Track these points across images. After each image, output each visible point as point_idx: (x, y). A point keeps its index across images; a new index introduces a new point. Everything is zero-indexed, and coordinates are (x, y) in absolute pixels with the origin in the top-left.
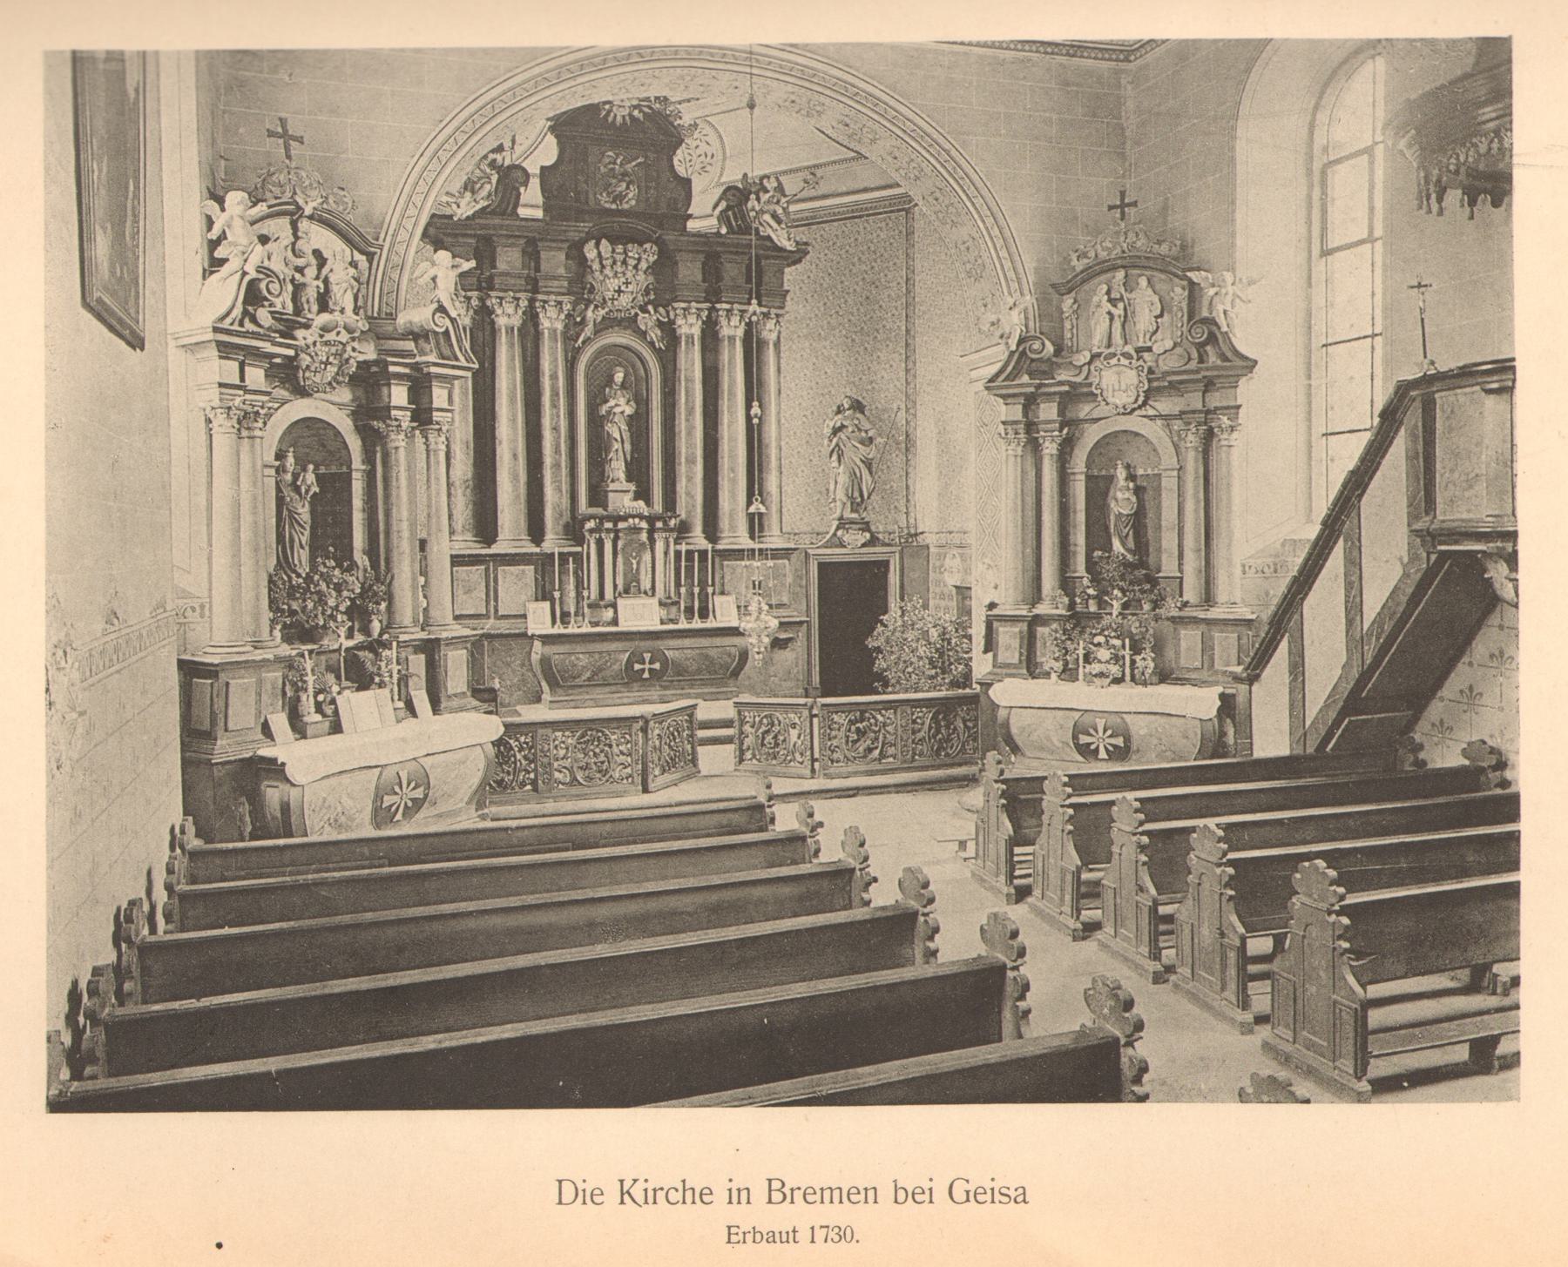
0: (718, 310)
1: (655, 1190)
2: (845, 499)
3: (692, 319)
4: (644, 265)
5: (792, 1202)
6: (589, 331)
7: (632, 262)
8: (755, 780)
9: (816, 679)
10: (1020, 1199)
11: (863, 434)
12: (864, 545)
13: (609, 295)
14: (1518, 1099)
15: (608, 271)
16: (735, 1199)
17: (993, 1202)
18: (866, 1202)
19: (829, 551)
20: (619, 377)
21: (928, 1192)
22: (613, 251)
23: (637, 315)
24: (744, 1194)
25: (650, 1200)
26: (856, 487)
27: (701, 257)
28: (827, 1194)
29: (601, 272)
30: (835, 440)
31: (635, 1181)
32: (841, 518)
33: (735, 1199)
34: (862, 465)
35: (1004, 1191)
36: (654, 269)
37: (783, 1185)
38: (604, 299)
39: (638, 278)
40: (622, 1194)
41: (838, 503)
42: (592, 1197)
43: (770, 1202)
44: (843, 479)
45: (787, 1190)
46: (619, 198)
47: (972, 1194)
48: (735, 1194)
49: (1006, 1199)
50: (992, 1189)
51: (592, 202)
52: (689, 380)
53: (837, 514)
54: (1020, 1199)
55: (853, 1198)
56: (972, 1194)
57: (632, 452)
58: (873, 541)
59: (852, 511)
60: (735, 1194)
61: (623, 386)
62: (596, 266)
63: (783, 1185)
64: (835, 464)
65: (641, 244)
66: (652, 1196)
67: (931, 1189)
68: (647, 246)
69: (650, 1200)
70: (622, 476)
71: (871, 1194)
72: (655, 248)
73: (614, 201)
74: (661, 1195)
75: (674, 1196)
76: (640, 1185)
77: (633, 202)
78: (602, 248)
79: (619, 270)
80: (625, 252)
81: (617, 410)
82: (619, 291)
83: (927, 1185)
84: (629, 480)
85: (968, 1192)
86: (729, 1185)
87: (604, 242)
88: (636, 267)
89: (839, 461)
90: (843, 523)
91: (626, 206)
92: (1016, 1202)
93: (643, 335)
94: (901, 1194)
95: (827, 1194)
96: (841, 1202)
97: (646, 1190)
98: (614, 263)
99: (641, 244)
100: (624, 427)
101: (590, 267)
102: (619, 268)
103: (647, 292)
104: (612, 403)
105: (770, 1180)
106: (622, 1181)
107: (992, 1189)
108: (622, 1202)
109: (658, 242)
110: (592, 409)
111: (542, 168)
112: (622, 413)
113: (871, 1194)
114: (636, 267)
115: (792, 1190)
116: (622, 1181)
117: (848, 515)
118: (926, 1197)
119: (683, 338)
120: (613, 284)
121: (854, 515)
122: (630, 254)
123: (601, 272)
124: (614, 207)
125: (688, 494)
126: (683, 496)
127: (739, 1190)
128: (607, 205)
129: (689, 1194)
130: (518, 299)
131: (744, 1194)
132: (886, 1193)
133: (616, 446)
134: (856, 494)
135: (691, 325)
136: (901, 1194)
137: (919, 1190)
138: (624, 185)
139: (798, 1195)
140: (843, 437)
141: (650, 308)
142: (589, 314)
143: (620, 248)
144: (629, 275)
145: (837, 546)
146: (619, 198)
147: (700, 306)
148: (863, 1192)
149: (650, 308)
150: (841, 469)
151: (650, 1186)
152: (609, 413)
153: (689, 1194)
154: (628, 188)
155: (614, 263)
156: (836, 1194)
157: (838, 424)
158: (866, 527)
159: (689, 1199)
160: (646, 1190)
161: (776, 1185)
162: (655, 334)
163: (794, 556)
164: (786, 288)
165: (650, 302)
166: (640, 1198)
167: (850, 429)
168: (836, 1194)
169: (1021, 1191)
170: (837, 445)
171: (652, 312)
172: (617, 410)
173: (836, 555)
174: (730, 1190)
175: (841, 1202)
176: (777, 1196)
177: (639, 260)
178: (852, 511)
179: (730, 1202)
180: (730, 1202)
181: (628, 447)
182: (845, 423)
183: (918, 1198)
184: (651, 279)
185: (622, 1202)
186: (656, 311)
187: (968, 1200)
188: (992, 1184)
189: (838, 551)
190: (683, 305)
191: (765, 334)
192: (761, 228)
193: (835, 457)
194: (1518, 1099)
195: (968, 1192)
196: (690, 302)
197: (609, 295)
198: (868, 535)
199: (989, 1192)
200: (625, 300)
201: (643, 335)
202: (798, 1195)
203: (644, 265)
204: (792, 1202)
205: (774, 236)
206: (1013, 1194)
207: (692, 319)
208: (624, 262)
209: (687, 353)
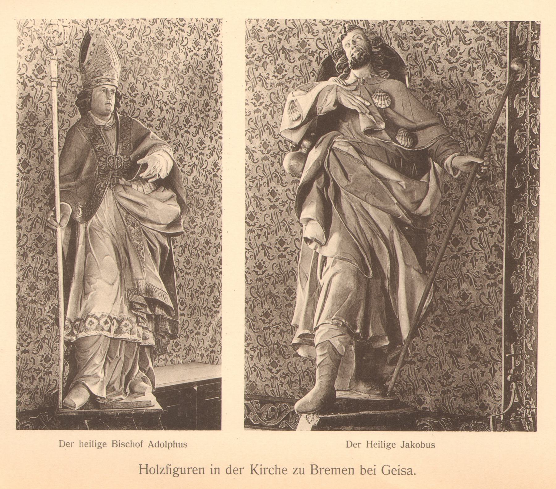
1: (265, 469)
8: (63, 164)
10: (409, 473)
11: (403, 141)
14: (534, 428)
16: (213, 472)
18: (200, 473)
24: (217, 470)
25: (263, 472)
28: (334, 470)
30: (314, 155)
31: (257, 465)
33: (213, 472)
35: (403, 470)
37: (317, 467)
40: (252, 470)
41: (319, 355)
42: (302, 472)
43: (312, 474)
45: (318, 469)
47: (391, 471)
49: (404, 473)
54: (409, 473)
56: (391, 471)
66: (265, 471)
69: (263, 472)
71: (202, 470)
74: (267, 471)
75: (272, 471)
76: (259, 467)
83: (373, 468)
85: (389, 470)
89: (326, 223)
94: (363, 471)
95: (334, 470)
97: (261, 469)
105: (312, 465)
106: (252, 465)
108: (252, 473)
113: (202, 470)
115: (321, 469)
116: (252, 465)
118: (373, 472)
127: (215, 469)
131: (217, 470)
132: (357, 470)
136: (363, 471)
137: (394, 470)
139: (323, 471)
151: (263, 467)
156: (338, 470)
159: (278, 472)
160: (261, 469)
161: (314, 467)
166: (259, 472)
168: (338, 470)
169: (410, 470)
176: (315, 471)
179: (212, 473)
180: (212, 473)
183: (345, 472)
185: (252, 473)
187: (389, 473)
188: (399, 467)
194: (534, 428)
202: (323, 471)
206: (407, 471)
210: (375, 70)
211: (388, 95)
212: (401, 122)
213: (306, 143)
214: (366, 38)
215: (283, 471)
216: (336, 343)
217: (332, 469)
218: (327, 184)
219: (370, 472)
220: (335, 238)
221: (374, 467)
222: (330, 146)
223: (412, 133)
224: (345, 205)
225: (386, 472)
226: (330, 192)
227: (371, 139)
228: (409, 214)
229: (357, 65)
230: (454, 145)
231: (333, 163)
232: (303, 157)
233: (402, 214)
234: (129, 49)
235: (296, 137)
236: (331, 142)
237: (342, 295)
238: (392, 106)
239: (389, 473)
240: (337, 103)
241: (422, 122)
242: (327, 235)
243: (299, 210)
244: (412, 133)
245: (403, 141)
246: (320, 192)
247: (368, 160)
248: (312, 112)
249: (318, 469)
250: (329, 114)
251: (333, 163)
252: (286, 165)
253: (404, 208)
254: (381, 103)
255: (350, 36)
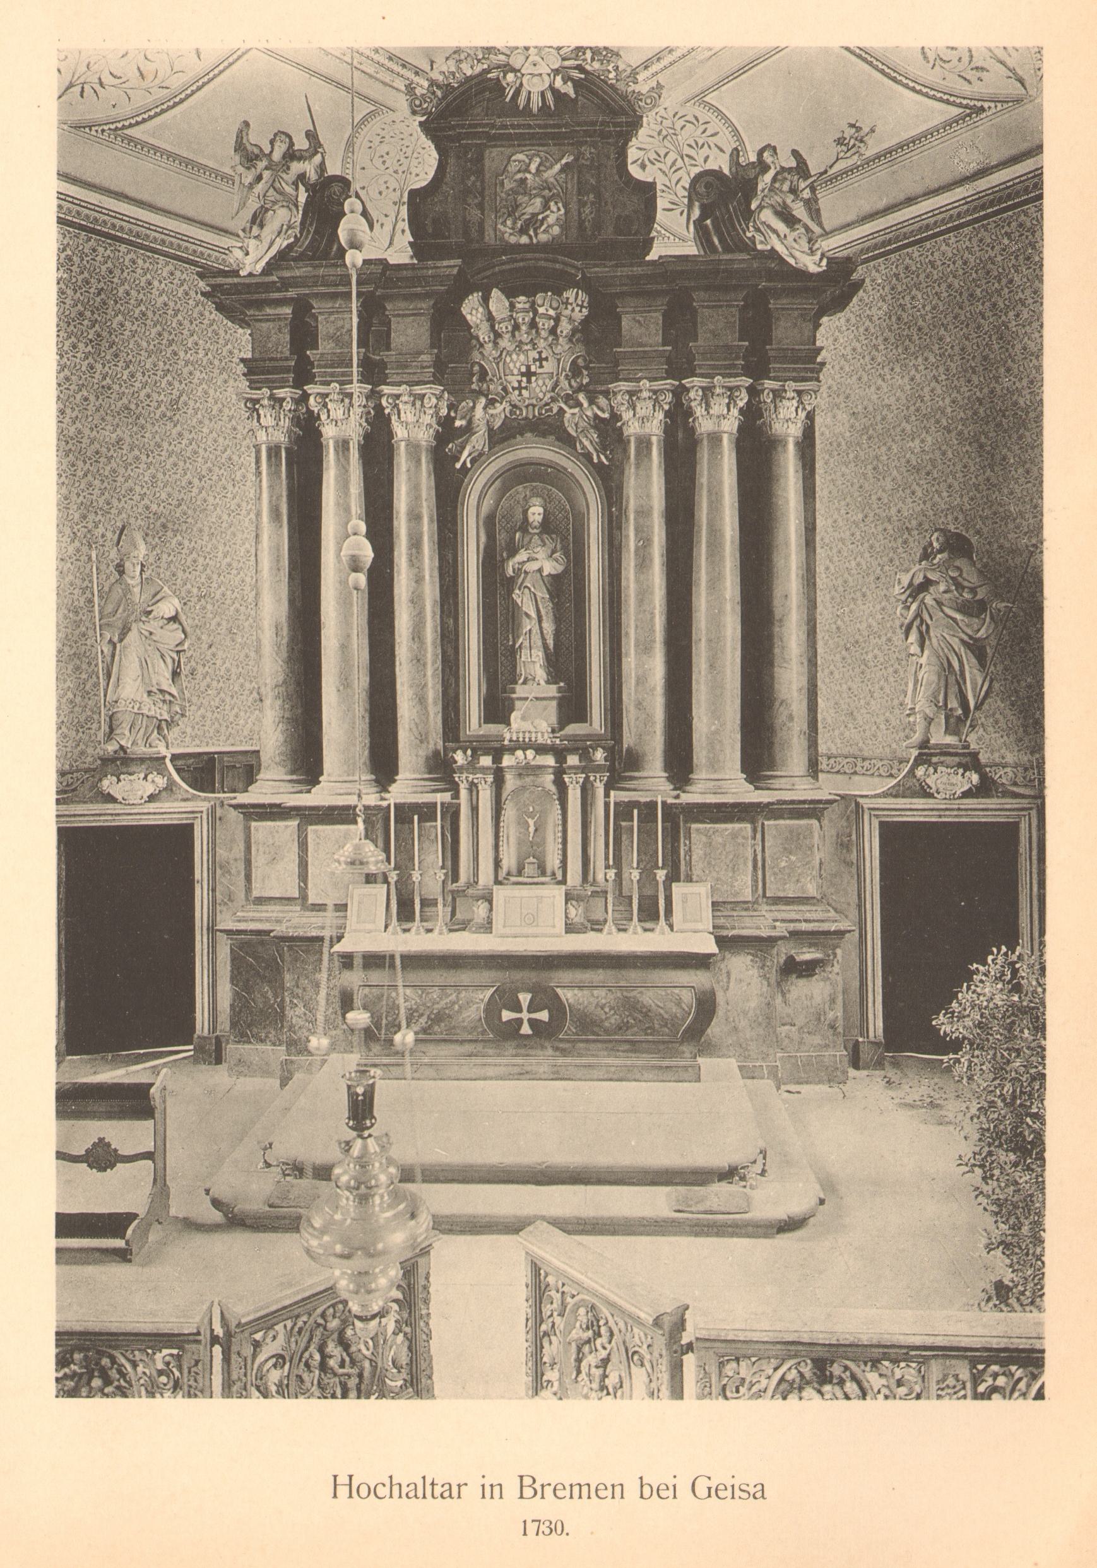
0: (688, 390)
2: (929, 712)
3: (644, 408)
4: (565, 327)
5: (543, 1497)
6: (478, 441)
7: (545, 324)
9: (877, 1025)
11: (967, 595)
12: (966, 794)
13: (514, 381)
15: (505, 343)
17: (733, 1497)
19: (901, 802)
20: (536, 513)
21: (671, 1488)
22: (512, 306)
23: (561, 411)
24: (497, 1490)
26: (953, 689)
27: (662, 303)
28: (576, 1489)
29: (496, 344)
30: (914, 607)
32: (924, 744)
34: (962, 651)
35: (743, 1487)
36: (584, 332)
37: (534, 1481)
38: (505, 389)
39: (558, 349)
41: (919, 718)
43: (521, 1497)
44: (928, 674)
45: (537, 1486)
46: (533, 223)
48: (488, 1489)
49: (745, 1495)
50: (733, 1486)
51: (489, 237)
52: (644, 513)
53: (917, 737)
54: (759, 1495)
55: (601, 1493)
57: (557, 634)
58: (985, 788)
59: (947, 731)
60: (488, 1489)
61: (546, 526)
62: (483, 334)
63: (534, 1481)
64: (914, 649)
65: (558, 292)
67: (674, 1486)
68: (570, 294)
70: (541, 674)
71: (618, 1489)
72: (583, 296)
73: (523, 231)
77: (556, 230)
78: (493, 306)
79: (525, 338)
80: (533, 308)
81: (532, 567)
82: (529, 374)
84: (552, 679)
85: (709, 1489)
86: (483, 1481)
87: (495, 293)
88: (553, 331)
89: (922, 646)
90: (926, 754)
91: (543, 237)
92: (755, 1498)
93: (567, 441)
94: (647, 1491)
95: (576, 1489)
96: (589, 1497)
98: (516, 327)
99: (558, 292)
100: (542, 594)
101: (477, 338)
102: (523, 335)
103: (576, 371)
104: (522, 556)
105: (521, 1477)
107: (733, 1486)
109: (586, 285)
110: (491, 564)
111: (413, 193)
112: (540, 570)
113: (618, 1489)
114: (553, 331)
115: (543, 1486)
117: (940, 737)
119: (632, 439)
120: (517, 362)
121: (950, 740)
122: (541, 310)
123: (496, 344)
124: (524, 240)
125: (639, 705)
126: (632, 708)
127: (492, 1486)
128: (513, 240)
129: (396, 1489)
130: (422, 397)
131: (497, 1490)
132: (632, 1489)
133: (527, 625)
134: (953, 703)
135: (643, 420)
136: (647, 1491)
138: (538, 201)
139: (549, 1491)
140: (929, 600)
141: (581, 397)
142: (479, 413)
143: (522, 301)
144: (542, 344)
145: (914, 795)
146: (533, 223)
147: (657, 385)
148: (610, 1488)
149: (581, 397)
150: (923, 660)
152: (518, 571)
153: (396, 1489)
154: (546, 207)
155: (516, 327)
156: (585, 1489)
157: (919, 579)
158: (971, 762)
161: (527, 1481)
162: (588, 442)
163: (829, 814)
164: (818, 344)
165: (581, 389)
167: (942, 587)
170: (918, 615)
171: (586, 404)
172: (532, 567)
173: (915, 810)
174: (483, 1486)
175: (589, 1497)
176: (528, 1492)
177: (557, 320)
178: (947, 731)
179: (483, 1497)
180: (483, 1497)
181: (549, 627)
182: (932, 576)
184: (580, 350)
186: (592, 402)
187: (709, 1496)
188: (733, 1481)
189: (920, 803)
190: (775, 385)
191: (778, 428)
192: (759, 238)
193: (913, 637)
195: (709, 1489)
196: (638, 380)
197: (514, 381)
198: (975, 778)
199: (730, 1489)
200: (540, 388)
201: (567, 441)
202: (549, 1491)
203: (565, 327)
204: (543, 1497)
205: (780, 248)
206: (752, 1490)
207: (644, 408)
208: (533, 325)
209: (638, 466)
210: (951, 552)
211: (958, 568)
212: (966, 584)
213: (910, 600)
214: (945, 535)
215: (452, 1492)
216: (927, 711)
217: (571, 1486)
218: (921, 624)
219: (663, 1494)
220: (926, 652)
221: (674, 1481)
222: (922, 601)
223: (973, 590)
224: (932, 634)
225: (702, 1491)
226: (924, 627)
227: (947, 596)
228: (971, 637)
229: (940, 551)
230: (998, 596)
231: (925, 611)
232: (908, 608)
233: (966, 638)
234: (177, 515)
235: (903, 597)
236: (924, 598)
237: (929, 684)
238: (961, 575)
239: (709, 1496)
240: (925, 577)
241: (977, 584)
242: (922, 651)
243: (907, 639)
244: (973, 590)
245: (967, 595)
246: (918, 628)
247: (945, 608)
248: (911, 584)
249: (537, 1486)
250: (921, 584)
251: (925, 611)
252: (898, 612)
253: (966, 634)
254: (954, 574)
255: (936, 535)
